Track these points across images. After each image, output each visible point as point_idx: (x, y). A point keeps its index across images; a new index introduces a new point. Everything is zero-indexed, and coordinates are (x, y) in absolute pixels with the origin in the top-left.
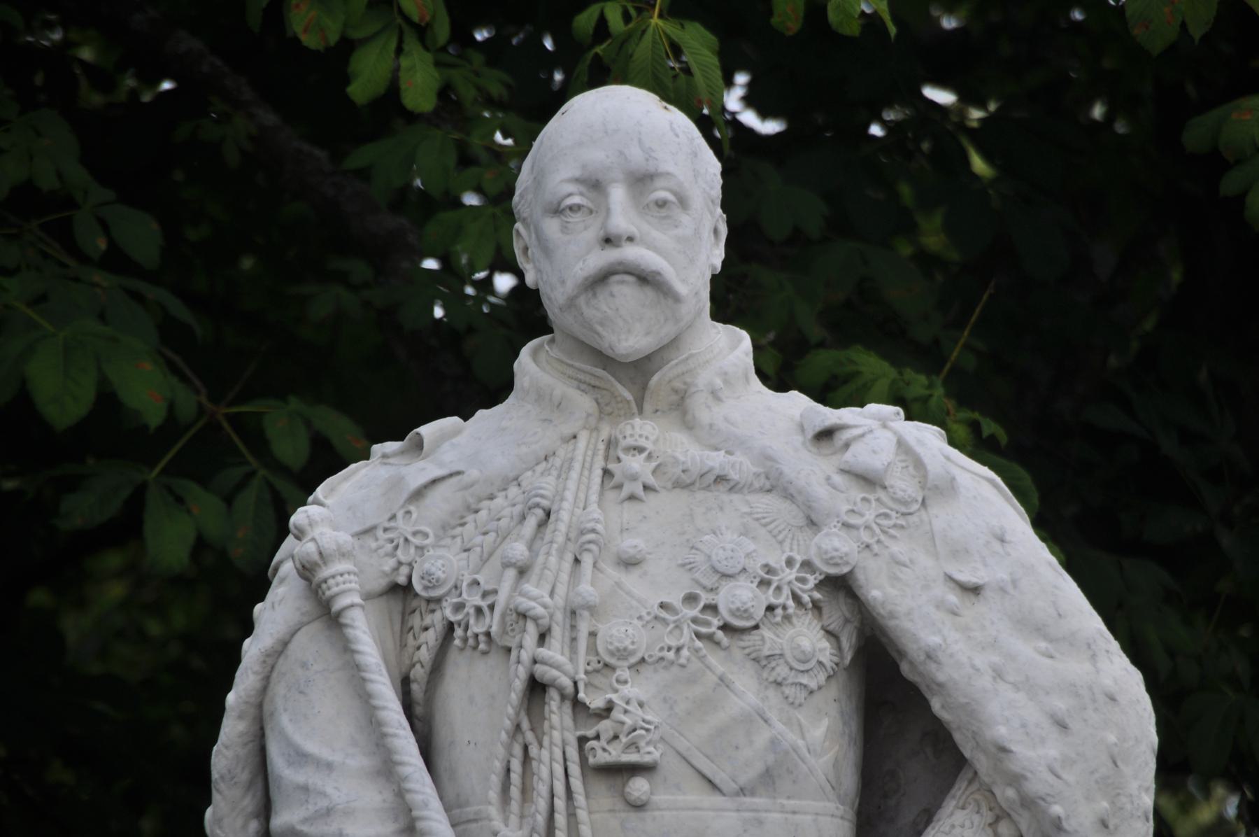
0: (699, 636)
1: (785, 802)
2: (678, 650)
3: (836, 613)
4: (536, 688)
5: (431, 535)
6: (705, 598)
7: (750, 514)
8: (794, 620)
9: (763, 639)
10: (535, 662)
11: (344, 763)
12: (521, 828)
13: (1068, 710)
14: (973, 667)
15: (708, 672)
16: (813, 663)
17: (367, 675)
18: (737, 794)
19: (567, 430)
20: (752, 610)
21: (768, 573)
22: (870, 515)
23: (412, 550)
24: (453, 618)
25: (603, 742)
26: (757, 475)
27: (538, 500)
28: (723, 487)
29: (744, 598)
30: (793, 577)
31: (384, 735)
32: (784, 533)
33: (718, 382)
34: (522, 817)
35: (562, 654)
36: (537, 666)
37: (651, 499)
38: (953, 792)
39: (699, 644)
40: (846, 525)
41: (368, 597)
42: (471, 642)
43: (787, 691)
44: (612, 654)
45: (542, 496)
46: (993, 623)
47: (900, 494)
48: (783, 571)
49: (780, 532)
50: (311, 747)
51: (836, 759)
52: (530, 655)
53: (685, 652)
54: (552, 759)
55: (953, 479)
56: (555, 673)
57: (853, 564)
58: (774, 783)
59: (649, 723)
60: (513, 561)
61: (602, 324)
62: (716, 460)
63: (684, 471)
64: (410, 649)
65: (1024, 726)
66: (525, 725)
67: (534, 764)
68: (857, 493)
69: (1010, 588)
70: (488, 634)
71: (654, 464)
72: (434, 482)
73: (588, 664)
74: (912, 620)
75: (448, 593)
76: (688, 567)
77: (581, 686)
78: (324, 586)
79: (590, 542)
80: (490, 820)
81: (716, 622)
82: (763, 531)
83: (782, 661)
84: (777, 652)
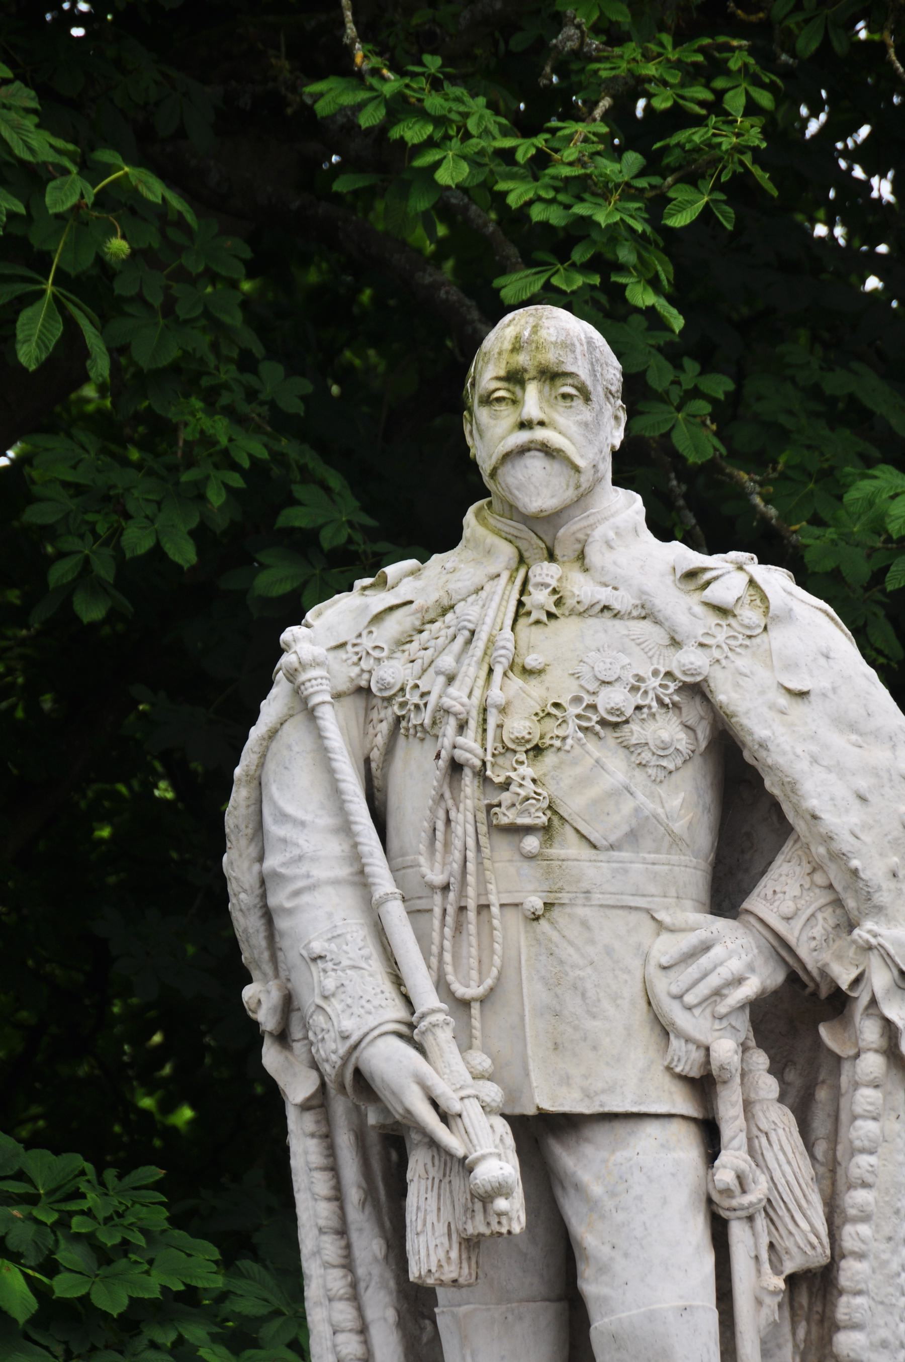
0: (581, 728)
1: (646, 856)
2: (564, 739)
3: (693, 712)
4: (456, 767)
5: (386, 649)
6: (588, 699)
7: (628, 636)
8: (657, 717)
9: (631, 732)
10: (455, 747)
11: (313, 822)
12: (442, 873)
13: (869, 787)
14: (795, 754)
15: (587, 756)
16: (672, 750)
17: (332, 756)
18: (607, 850)
19: (493, 570)
20: (623, 709)
21: (638, 681)
23: (372, 661)
24: (399, 713)
25: (503, 809)
27: (466, 623)
28: (607, 614)
29: (617, 700)
30: (657, 684)
31: (344, 801)
32: (653, 651)
33: (611, 535)
34: (444, 864)
35: (476, 741)
36: (456, 750)
37: (553, 624)
38: (783, 849)
39: (580, 735)
40: (702, 645)
41: (338, 696)
42: (412, 731)
44: (513, 741)
45: (469, 621)
46: (814, 720)
47: (746, 621)
48: (649, 679)
49: (650, 650)
50: (290, 809)
51: (690, 823)
52: (451, 742)
53: (569, 741)
54: (465, 821)
55: (791, 610)
56: (468, 755)
57: (706, 674)
58: (637, 840)
59: (539, 794)
60: (443, 670)
61: (518, 489)
62: (604, 595)
63: (578, 602)
64: (370, 736)
65: (832, 799)
66: (447, 795)
67: (453, 824)
68: (712, 619)
69: (830, 694)
70: (422, 725)
71: (557, 597)
72: (392, 609)
73: (495, 749)
74: (749, 718)
75: (395, 695)
76: (576, 676)
77: (489, 766)
78: (302, 687)
79: (501, 656)
80: (420, 866)
81: (595, 718)
82: (637, 650)
83: (646, 748)
84: (643, 741)
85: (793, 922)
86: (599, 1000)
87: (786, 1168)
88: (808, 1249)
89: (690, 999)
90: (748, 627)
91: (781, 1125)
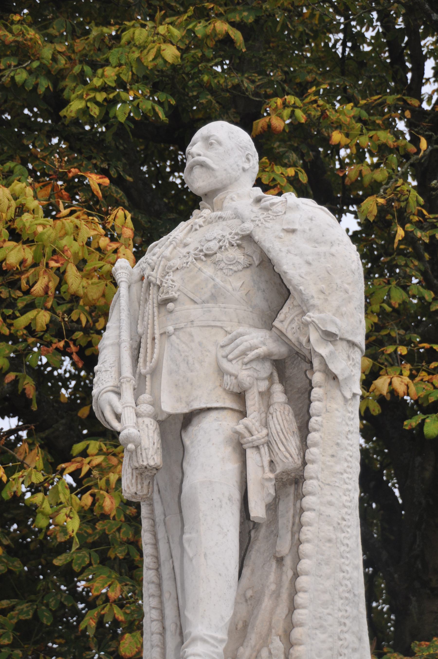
1: (221, 305)
2: (187, 263)
18: (202, 303)
22: (261, 217)
26: (232, 215)
43: (224, 271)
53: (189, 263)
85: (284, 323)
86: (194, 364)
87: (278, 427)
88: (284, 460)
89: (230, 357)
90: (276, 213)
91: (279, 410)
